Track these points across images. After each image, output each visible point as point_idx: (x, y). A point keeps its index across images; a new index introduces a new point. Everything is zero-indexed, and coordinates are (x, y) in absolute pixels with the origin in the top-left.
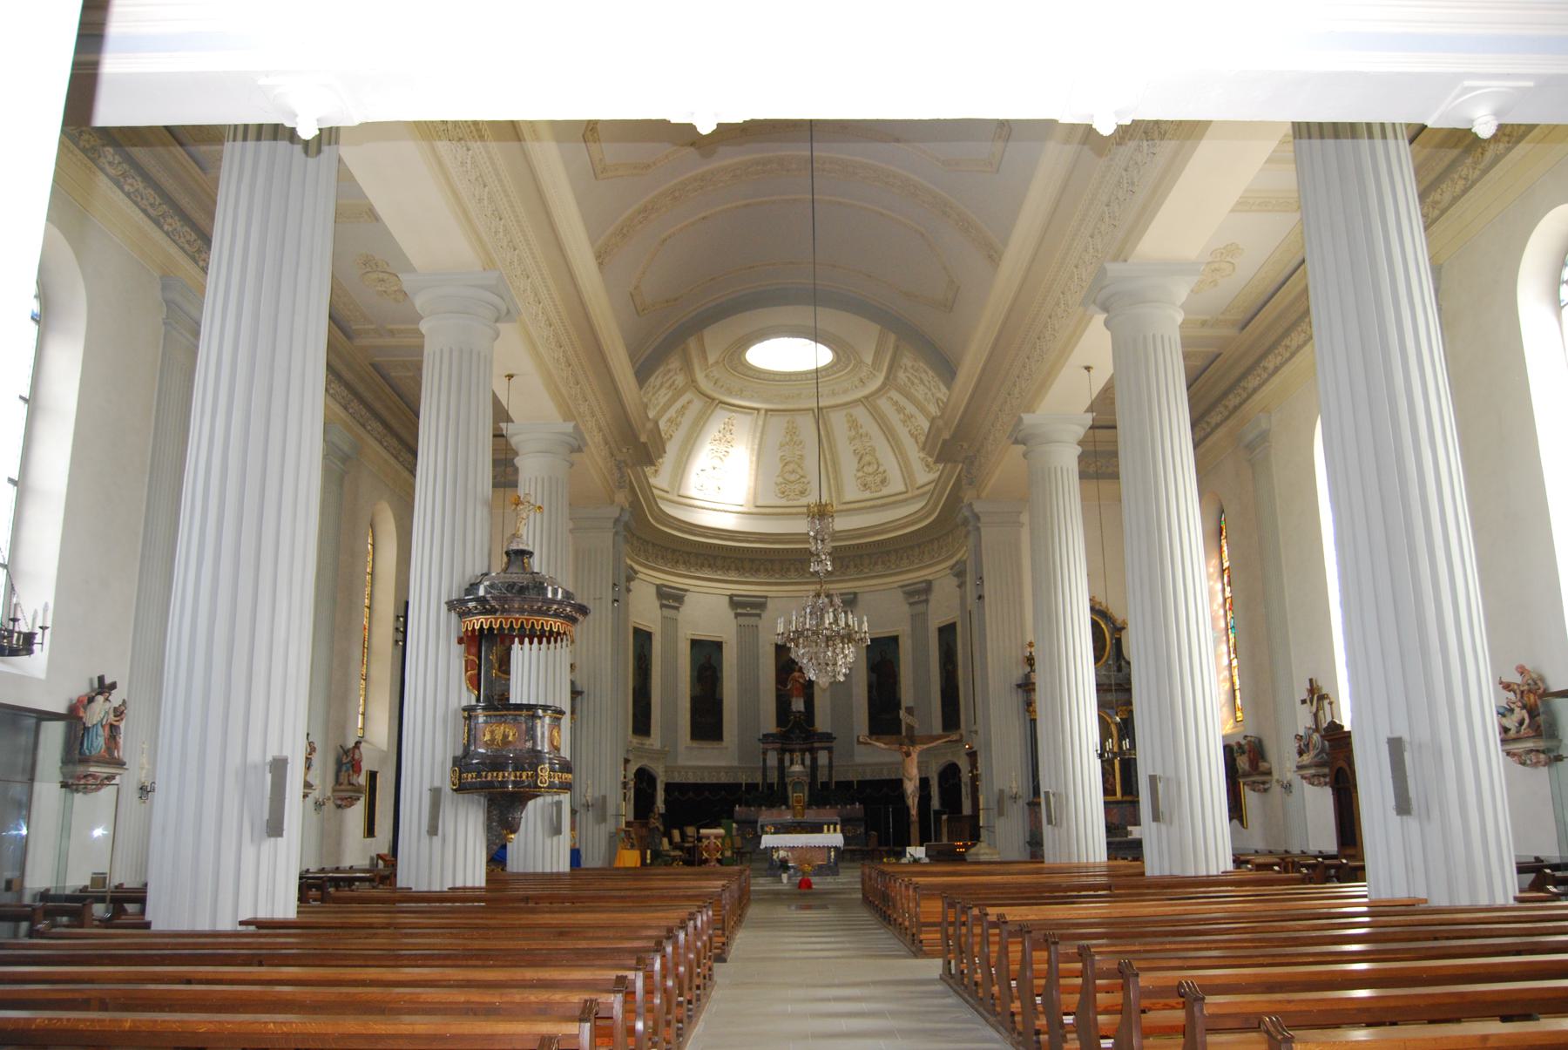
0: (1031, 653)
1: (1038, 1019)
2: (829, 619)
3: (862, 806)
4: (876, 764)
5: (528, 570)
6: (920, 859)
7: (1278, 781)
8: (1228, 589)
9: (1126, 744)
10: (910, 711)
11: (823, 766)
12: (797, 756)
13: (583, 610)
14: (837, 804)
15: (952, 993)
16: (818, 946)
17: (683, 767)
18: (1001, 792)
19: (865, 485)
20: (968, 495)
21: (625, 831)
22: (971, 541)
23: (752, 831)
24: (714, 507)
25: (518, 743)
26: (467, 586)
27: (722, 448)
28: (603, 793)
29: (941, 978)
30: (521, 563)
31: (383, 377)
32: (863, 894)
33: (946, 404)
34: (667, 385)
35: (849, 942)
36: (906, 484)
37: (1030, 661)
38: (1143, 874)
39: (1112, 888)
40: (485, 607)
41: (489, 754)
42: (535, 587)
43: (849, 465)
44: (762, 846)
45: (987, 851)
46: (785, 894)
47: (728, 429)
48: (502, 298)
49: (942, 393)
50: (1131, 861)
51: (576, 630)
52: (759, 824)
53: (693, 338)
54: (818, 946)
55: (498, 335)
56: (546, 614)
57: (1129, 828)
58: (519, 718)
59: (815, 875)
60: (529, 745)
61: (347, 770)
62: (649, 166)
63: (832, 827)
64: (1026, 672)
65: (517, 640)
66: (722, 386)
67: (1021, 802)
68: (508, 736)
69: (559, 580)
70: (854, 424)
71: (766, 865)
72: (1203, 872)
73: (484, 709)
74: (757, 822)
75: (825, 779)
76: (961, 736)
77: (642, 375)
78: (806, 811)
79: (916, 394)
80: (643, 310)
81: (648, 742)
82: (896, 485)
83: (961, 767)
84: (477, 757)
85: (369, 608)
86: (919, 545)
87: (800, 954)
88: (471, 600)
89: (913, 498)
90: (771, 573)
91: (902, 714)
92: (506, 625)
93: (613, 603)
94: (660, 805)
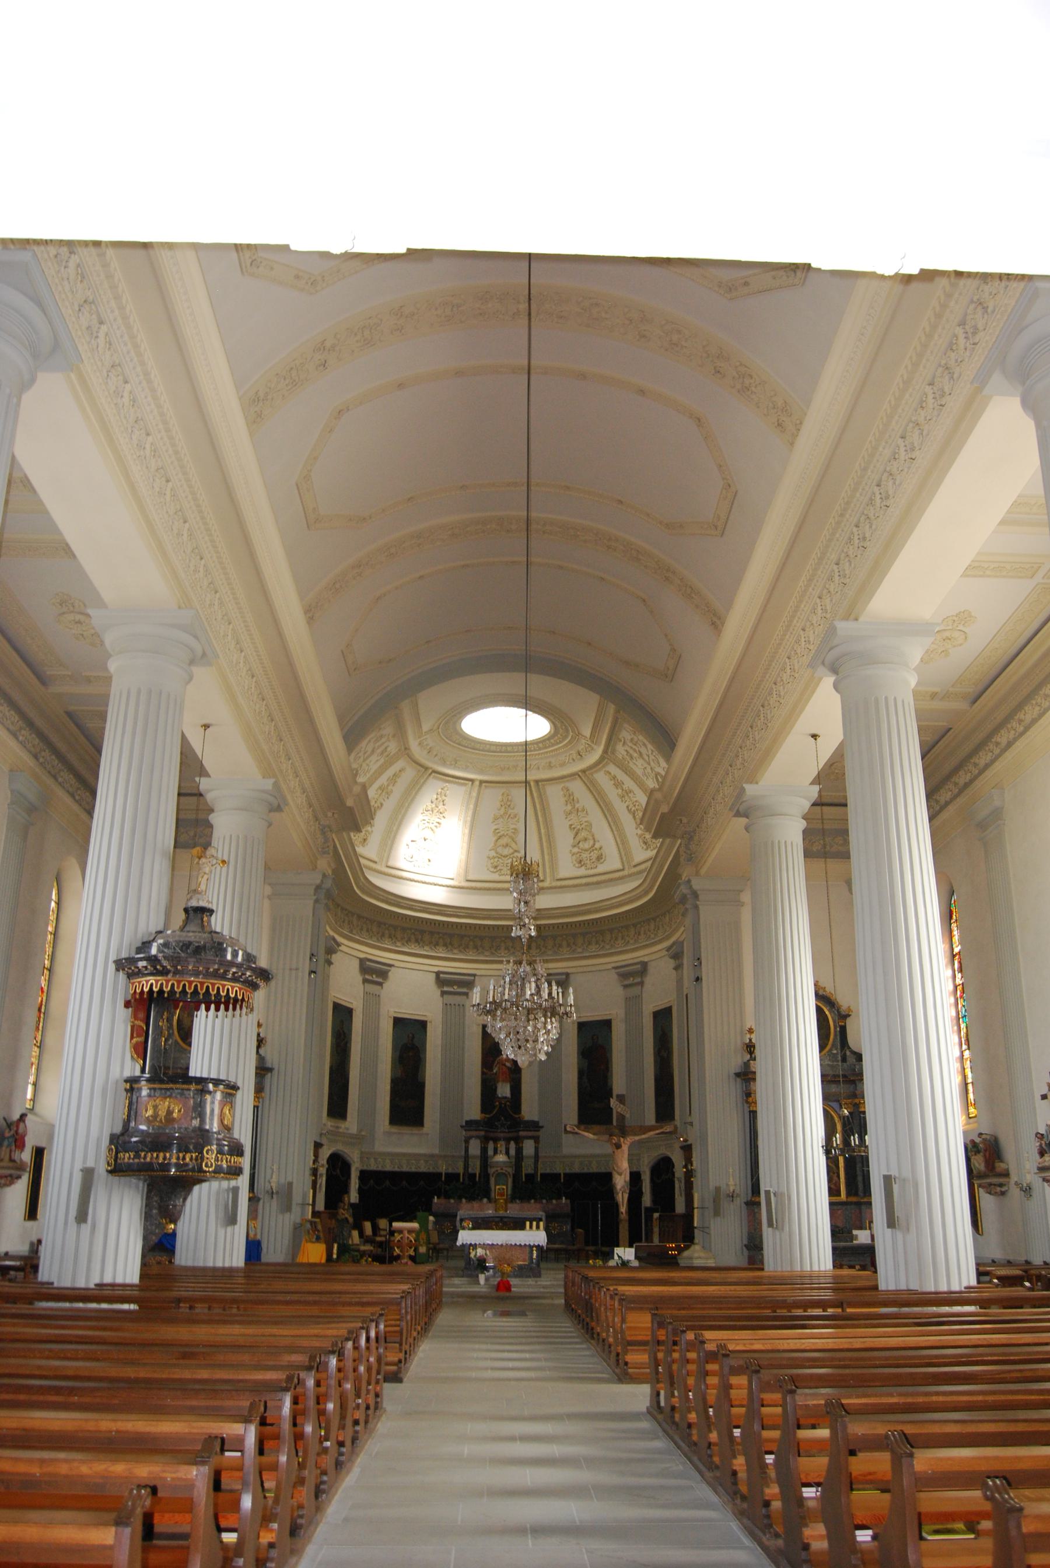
0: (750, 1040)
1: (768, 1486)
2: (530, 989)
3: (568, 1201)
4: (584, 1156)
5: (207, 929)
6: (629, 1261)
7: (1016, 1184)
8: (959, 976)
9: (855, 1140)
10: (621, 1099)
11: (475, 1157)
12: (502, 1145)
13: (265, 975)
14: (542, 1198)
15: (661, 1433)
16: (510, 1364)
17: (384, 1154)
18: (718, 1189)
19: (581, 861)
20: (686, 873)
21: (311, 1223)
22: (688, 920)
23: (449, 1225)
24: (423, 880)
25: (183, 1120)
26: (139, 944)
27: (435, 819)
28: (289, 1179)
29: (649, 1412)
30: (200, 921)
31: (78, 726)
32: (566, 1301)
33: (664, 778)
34: (379, 751)
35: (546, 1360)
36: (623, 863)
37: (750, 1048)
38: (875, 1288)
39: (845, 1306)
40: (156, 967)
41: (150, 1131)
42: (213, 947)
43: (564, 840)
44: (459, 1243)
45: (702, 1255)
46: (481, 1297)
47: (441, 800)
48: (196, 637)
49: (661, 767)
50: (859, 1270)
51: (259, 997)
52: (458, 1218)
53: (407, 701)
54: (510, 1364)
55: (191, 678)
56: (223, 977)
57: (855, 1232)
58: (186, 1092)
59: (516, 1276)
60: (196, 1123)
61: (9, 1145)
62: (364, 519)
63: (534, 1223)
64: (745, 1060)
65: (203, 1006)
66: (436, 755)
67: (739, 1202)
68: (172, 1112)
69: (242, 940)
70: (570, 798)
71: (462, 1264)
72: (944, 1288)
73: (148, 1080)
74: (456, 1216)
75: (530, 1171)
76: (676, 1127)
77: (353, 736)
78: (510, 1205)
79: (634, 767)
80: (355, 669)
81: (343, 1126)
82: (613, 862)
83: (674, 1160)
84: (136, 1134)
85: (50, 970)
86: (635, 925)
87: (489, 1374)
88: (141, 959)
89: (630, 875)
90: (481, 950)
91: (613, 1102)
92: (178, 987)
93: (310, 975)
94: (354, 1196)
